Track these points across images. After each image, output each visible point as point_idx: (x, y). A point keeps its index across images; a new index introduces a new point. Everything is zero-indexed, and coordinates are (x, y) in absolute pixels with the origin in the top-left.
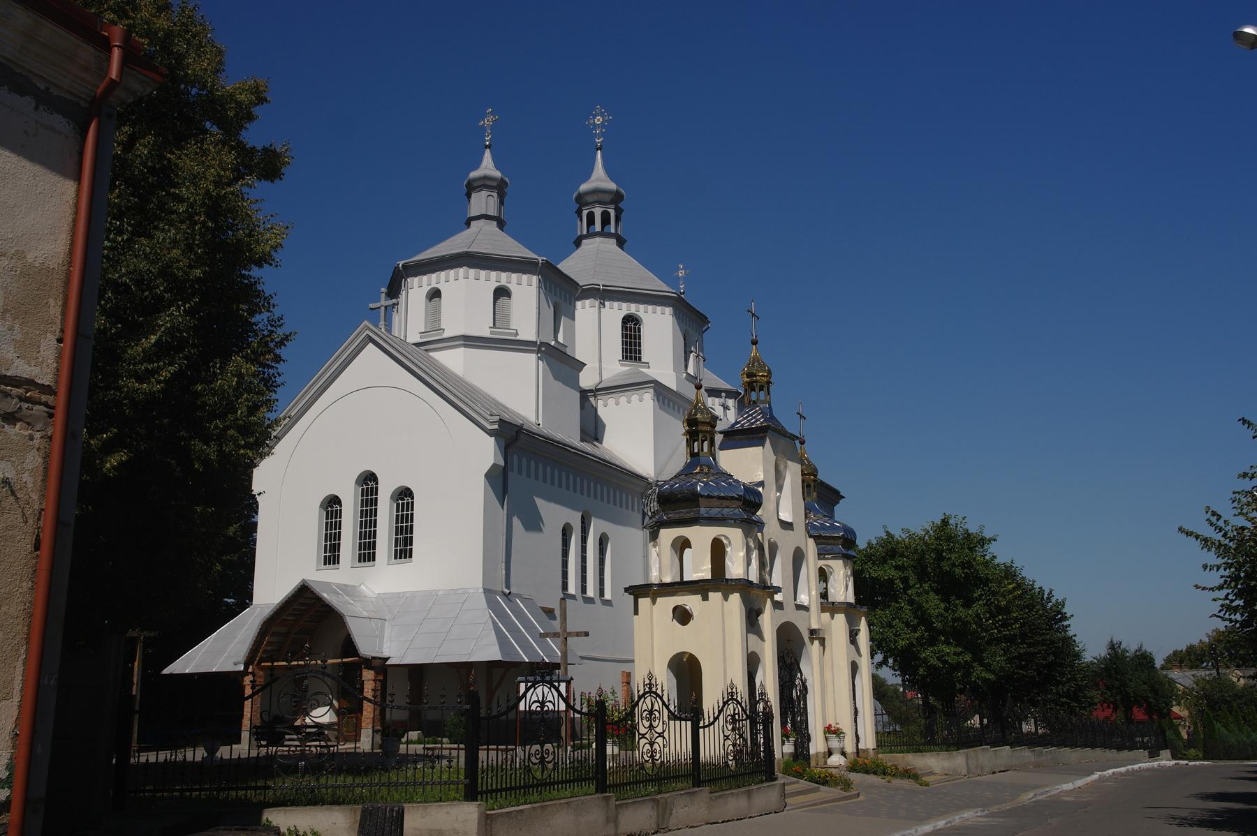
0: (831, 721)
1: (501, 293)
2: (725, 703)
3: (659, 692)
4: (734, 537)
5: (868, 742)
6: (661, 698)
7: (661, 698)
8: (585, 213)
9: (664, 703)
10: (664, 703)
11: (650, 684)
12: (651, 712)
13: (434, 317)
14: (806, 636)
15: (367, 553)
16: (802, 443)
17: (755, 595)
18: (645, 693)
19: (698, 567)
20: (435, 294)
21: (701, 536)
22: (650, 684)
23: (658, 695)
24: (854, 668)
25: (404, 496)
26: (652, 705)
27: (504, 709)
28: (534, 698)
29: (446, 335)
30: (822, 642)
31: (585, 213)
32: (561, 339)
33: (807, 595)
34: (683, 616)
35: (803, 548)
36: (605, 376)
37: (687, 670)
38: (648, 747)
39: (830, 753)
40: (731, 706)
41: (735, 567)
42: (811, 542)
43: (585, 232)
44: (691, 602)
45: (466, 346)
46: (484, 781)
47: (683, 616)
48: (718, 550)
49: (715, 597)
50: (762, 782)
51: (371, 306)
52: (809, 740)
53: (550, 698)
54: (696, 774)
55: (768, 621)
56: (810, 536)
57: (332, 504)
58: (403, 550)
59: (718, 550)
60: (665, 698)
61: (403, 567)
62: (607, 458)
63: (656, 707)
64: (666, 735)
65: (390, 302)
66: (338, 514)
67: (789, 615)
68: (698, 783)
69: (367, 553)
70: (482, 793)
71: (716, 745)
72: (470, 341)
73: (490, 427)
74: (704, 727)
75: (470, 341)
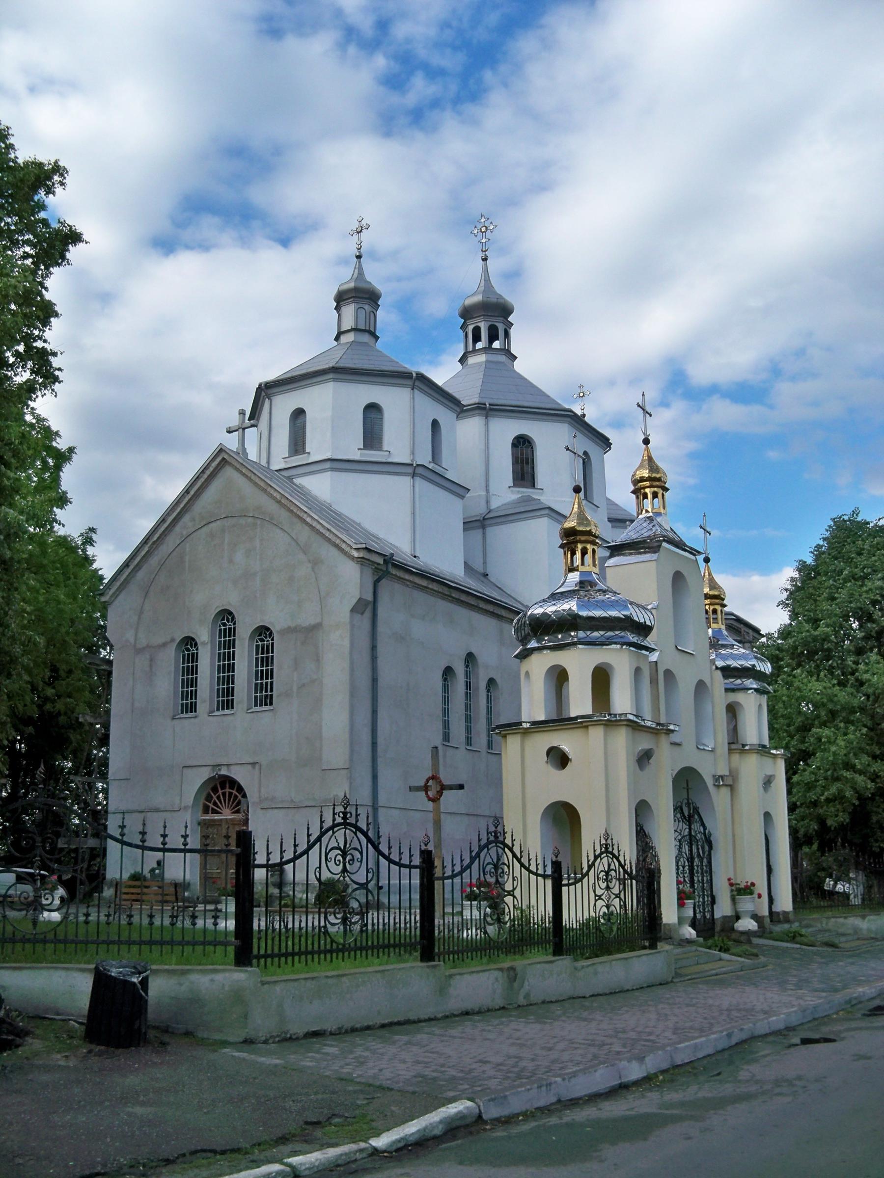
1: (372, 410)
2: (596, 857)
3: (616, 852)
4: (620, 661)
5: (785, 902)
6: (511, 850)
7: (511, 850)
9: (514, 855)
10: (514, 855)
11: (495, 832)
12: (607, 873)
14: (709, 782)
15: (226, 699)
16: (707, 560)
17: (650, 732)
18: (489, 842)
20: (299, 413)
21: (579, 663)
22: (495, 832)
23: (614, 855)
26: (609, 865)
27: (289, 855)
28: (333, 844)
30: (732, 787)
31: (471, 328)
33: (716, 736)
34: (559, 759)
35: (707, 681)
36: (494, 504)
37: (564, 817)
38: (605, 909)
39: (738, 918)
40: (605, 860)
41: (622, 701)
44: (565, 741)
46: (258, 947)
47: (559, 759)
48: (601, 679)
49: (597, 733)
50: (644, 948)
53: (355, 844)
54: (558, 939)
55: (667, 763)
58: (264, 697)
59: (601, 679)
60: (621, 859)
61: (265, 717)
62: (737, 713)
63: (612, 867)
64: (517, 893)
66: (194, 658)
67: (690, 758)
68: (558, 950)
69: (226, 699)
70: (258, 957)
71: (582, 905)
72: (337, 464)
73: (356, 554)
74: (568, 885)
75: (337, 464)
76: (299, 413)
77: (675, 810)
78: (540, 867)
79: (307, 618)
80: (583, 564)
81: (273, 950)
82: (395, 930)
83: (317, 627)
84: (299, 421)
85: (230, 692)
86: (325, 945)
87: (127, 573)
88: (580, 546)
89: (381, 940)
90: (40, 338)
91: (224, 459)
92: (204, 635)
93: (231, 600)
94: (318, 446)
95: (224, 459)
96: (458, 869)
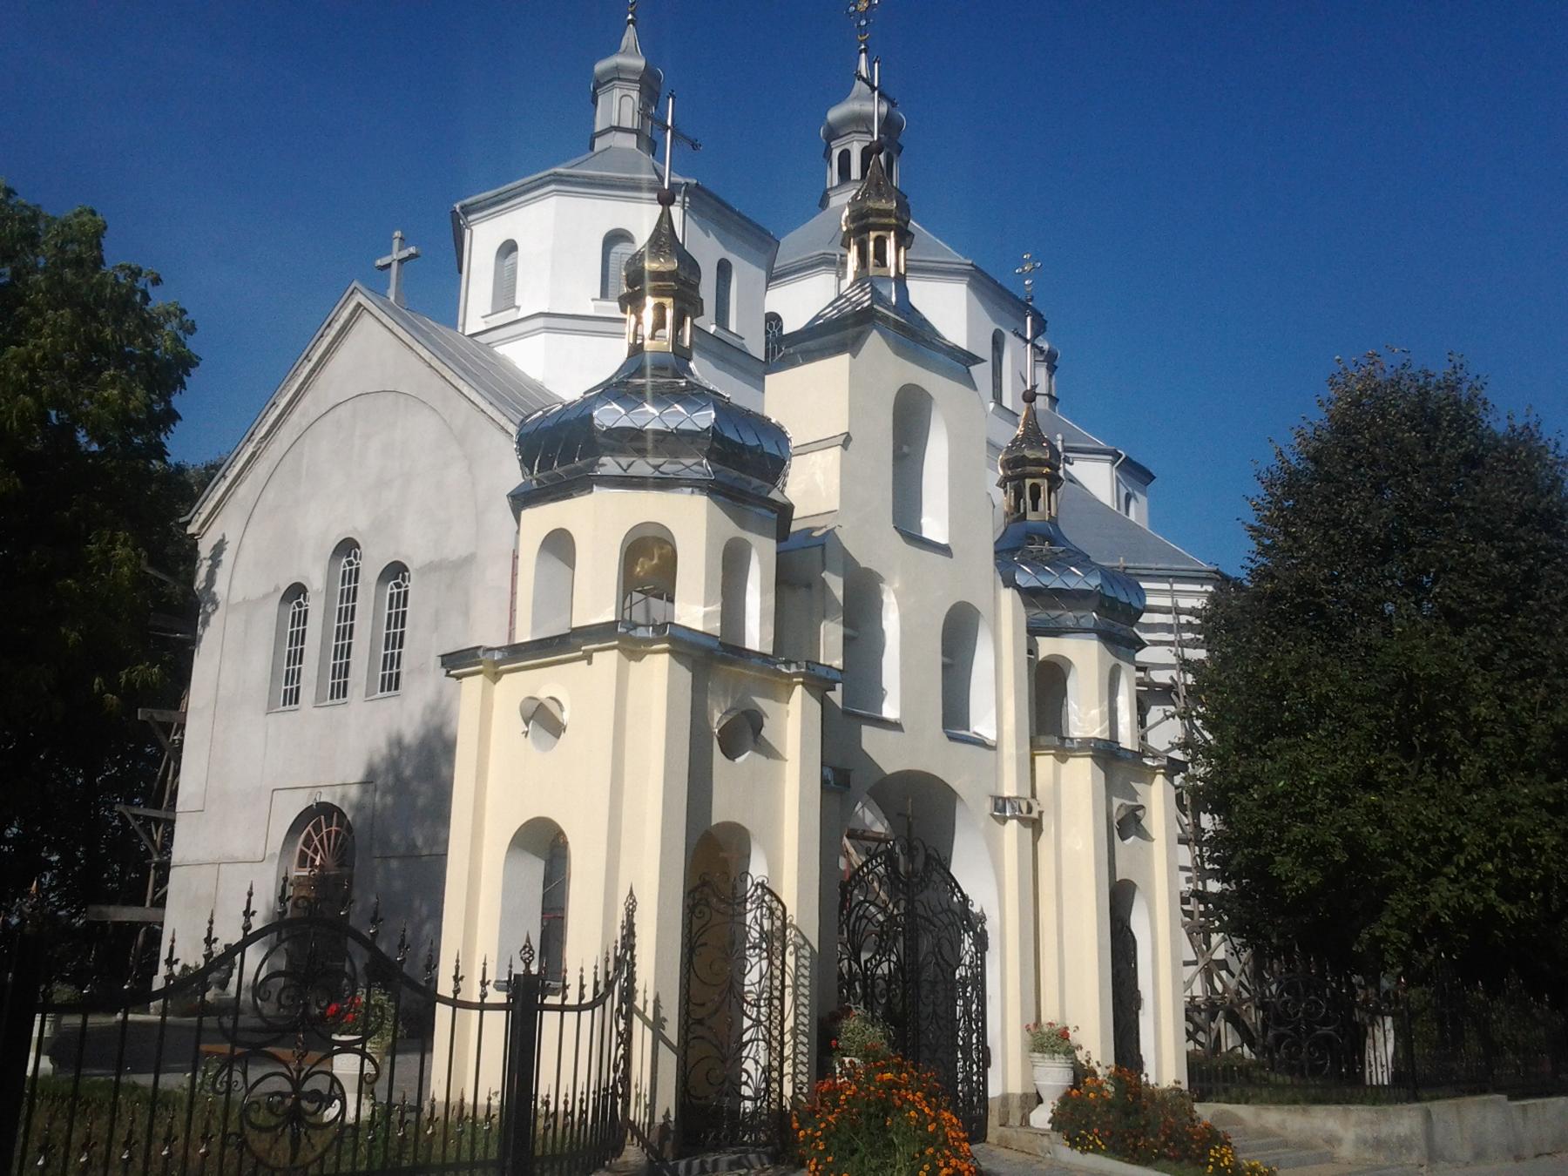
0: (1050, 1014)
5: (1164, 1060)
8: (836, 153)
13: (505, 293)
19: (596, 598)
20: (509, 248)
24: (1120, 897)
25: (396, 571)
29: (521, 315)
30: (1035, 825)
31: (836, 153)
32: (733, 328)
34: (543, 719)
41: (693, 609)
42: (1008, 597)
43: (836, 182)
45: (548, 329)
47: (543, 719)
51: (379, 263)
52: (986, 1061)
56: (1009, 582)
57: (296, 592)
58: (392, 683)
65: (404, 254)
66: (302, 618)
72: (557, 321)
76: (509, 248)
77: (1189, 935)
78: (650, 1006)
79: (455, 547)
80: (1035, 508)
81: (486, 1152)
82: (565, 1127)
83: (468, 561)
84: (508, 261)
85: (345, 671)
86: (473, 1149)
87: (223, 489)
88: (1028, 482)
89: (480, 1147)
90: (1183, 644)
91: (359, 305)
92: (316, 582)
93: (356, 524)
94: (530, 298)
95: (359, 305)
96: (588, 998)
